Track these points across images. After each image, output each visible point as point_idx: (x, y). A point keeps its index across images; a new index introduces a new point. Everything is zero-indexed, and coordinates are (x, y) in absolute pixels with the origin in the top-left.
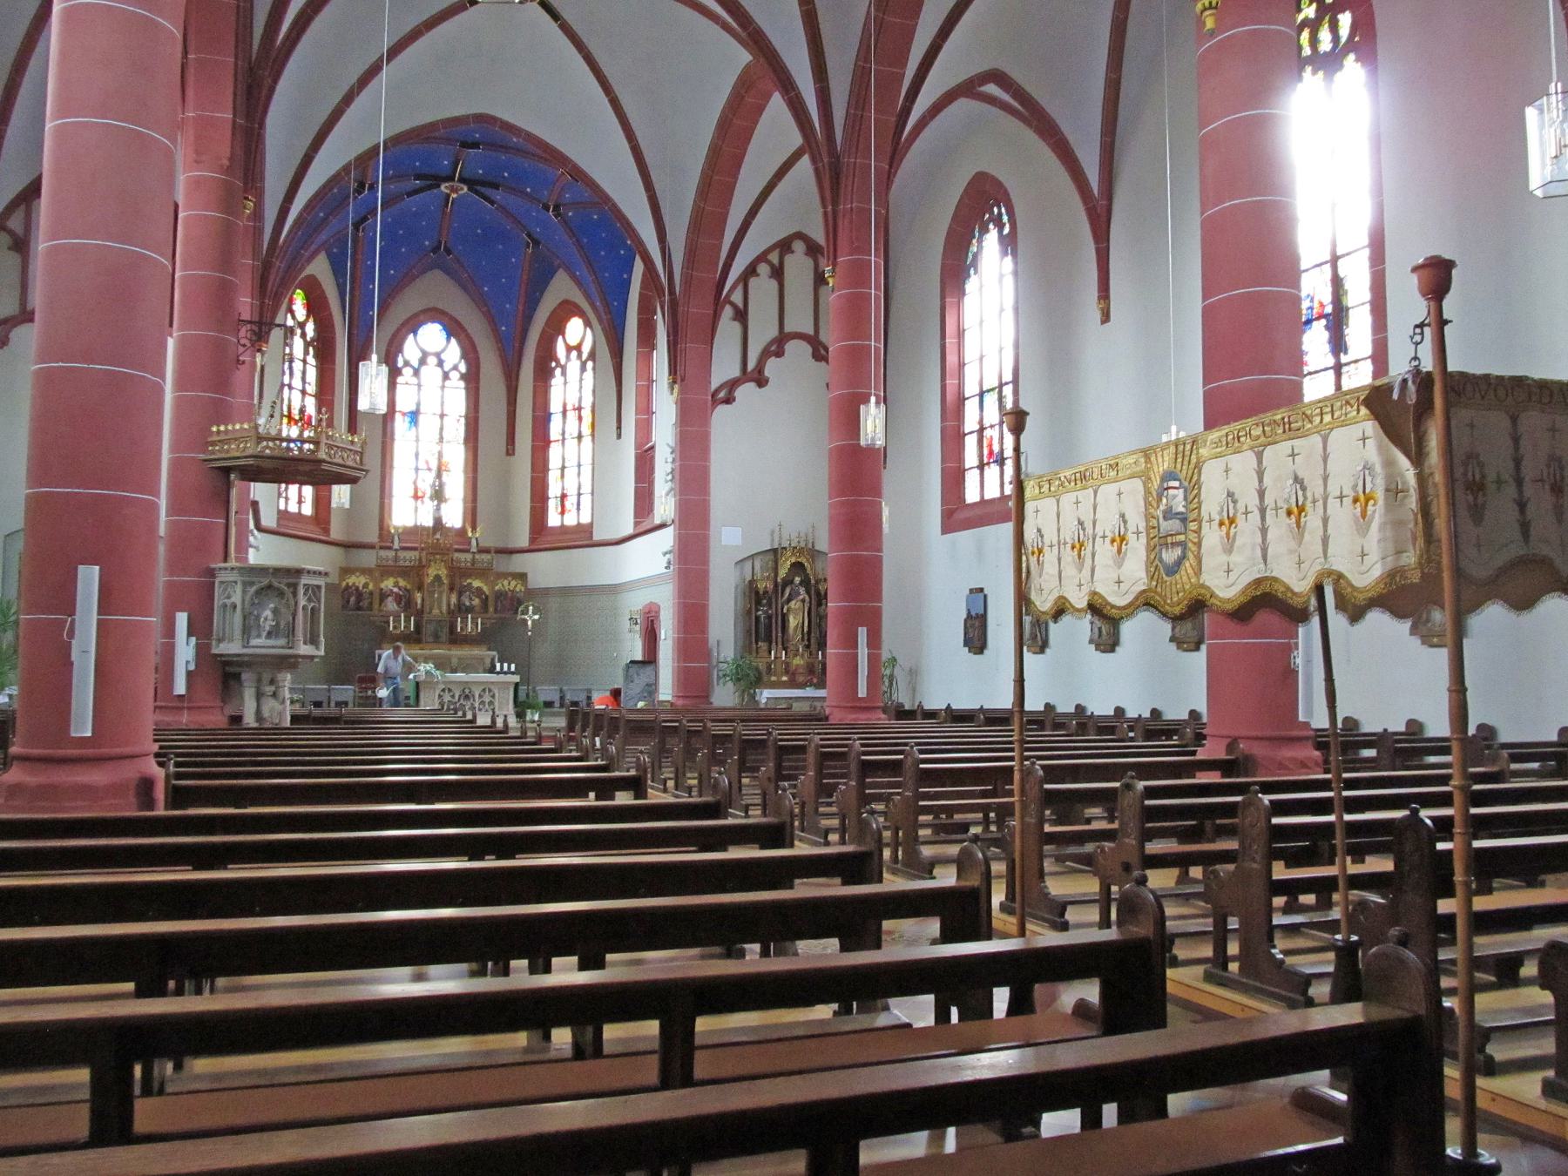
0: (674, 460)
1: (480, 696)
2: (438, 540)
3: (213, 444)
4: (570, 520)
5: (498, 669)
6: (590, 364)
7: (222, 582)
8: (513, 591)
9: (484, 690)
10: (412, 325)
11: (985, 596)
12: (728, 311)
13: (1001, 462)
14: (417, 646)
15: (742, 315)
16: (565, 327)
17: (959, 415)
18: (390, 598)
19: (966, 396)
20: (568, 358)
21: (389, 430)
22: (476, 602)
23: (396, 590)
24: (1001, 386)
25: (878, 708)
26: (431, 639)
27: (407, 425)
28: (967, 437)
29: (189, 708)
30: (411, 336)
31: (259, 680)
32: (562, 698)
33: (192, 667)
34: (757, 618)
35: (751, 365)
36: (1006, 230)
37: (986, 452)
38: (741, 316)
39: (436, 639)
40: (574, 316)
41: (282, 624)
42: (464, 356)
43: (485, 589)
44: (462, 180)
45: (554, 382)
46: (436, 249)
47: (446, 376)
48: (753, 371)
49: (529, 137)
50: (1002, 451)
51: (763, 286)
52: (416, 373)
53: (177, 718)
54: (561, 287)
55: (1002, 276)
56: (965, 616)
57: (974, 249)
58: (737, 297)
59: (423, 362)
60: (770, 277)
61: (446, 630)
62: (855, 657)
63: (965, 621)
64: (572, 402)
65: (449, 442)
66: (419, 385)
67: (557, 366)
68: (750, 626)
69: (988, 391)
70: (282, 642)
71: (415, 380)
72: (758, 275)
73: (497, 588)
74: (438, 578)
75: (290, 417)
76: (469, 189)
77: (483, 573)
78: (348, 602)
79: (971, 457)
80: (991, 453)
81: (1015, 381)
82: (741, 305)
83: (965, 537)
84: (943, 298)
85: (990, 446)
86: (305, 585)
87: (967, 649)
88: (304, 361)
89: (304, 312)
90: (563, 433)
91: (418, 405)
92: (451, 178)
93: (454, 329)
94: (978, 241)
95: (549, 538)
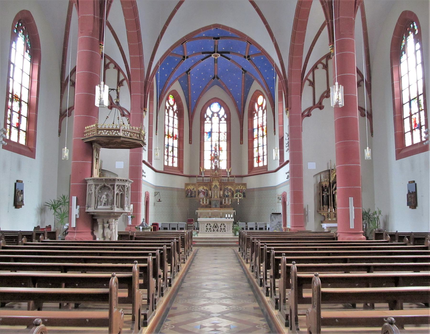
0: (288, 138)
1: (220, 226)
2: (216, 173)
3: (85, 133)
4: (261, 164)
5: (226, 216)
6: (265, 111)
7: (89, 185)
8: (242, 190)
9: (222, 224)
10: (209, 104)
11: (416, 184)
12: (307, 83)
13: (420, 127)
14: (210, 209)
15: (312, 84)
16: (257, 99)
17: (401, 112)
18: (201, 193)
19: (404, 103)
20: (259, 110)
21: (202, 139)
22: (230, 193)
23: (203, 190)
24: (418, 96)
25: (361, 233)
26: (214, 206)
27: (208, 136)
28: (405, 120)
29: (77, 232)
30: (209, 108)
31: (103, 223)
32: (256, 226)
33: (78, 217)
34: (323, 196)
35: (317, 101)
36: (417, 32)
37: (413, 124)
38: (312, 84)
39: (216, 206)
40: (260, 95)
41: (110, 200)
42: (226, 113)
43: (233, 189)
44: (218, 52)
45: (255, 118)
46: (214, 78)
47: (220, 120)
48: (318, 103)
49: (232, 30)
50: (420, 123)
51: (320, 73)
52: (211, 119)
53: (72, 236)
54: (256, 86)
55: (416, 51)
56: (407, 193)
57: (403, 44)
58: (310, 77)
59: (213, 115)
60: (323, 69)
61: (219, 203)
62: (348, 210)
63: (407, 195)
64: (260, 123)
65: (222, 141)
66: (212, 123)
67: (255, 113)
68: (320, 200)
69: (413, 99)
70: (109, 207)
71: (210, 122)
72: (318, 68)
73: (236, 189)
74: (216, 186)
75: (169, 136)
76: (221, 55)
77: (232, 184)
78: (188, 195)
79: (407, 128)
80: (416, 124)
81: (424, 94)
82: (312, 80)
83: (406, 160)
84: (392, 65)
85: (415, 121)
86: (117, 185)
87: (409, 207)
88: (173, 118)
89: (173, 102)
90: (258, 135)
91: (212, 129)
92: (214, 52)
93: (222, 104)
94: (405, 41)
95: (254, 171)
